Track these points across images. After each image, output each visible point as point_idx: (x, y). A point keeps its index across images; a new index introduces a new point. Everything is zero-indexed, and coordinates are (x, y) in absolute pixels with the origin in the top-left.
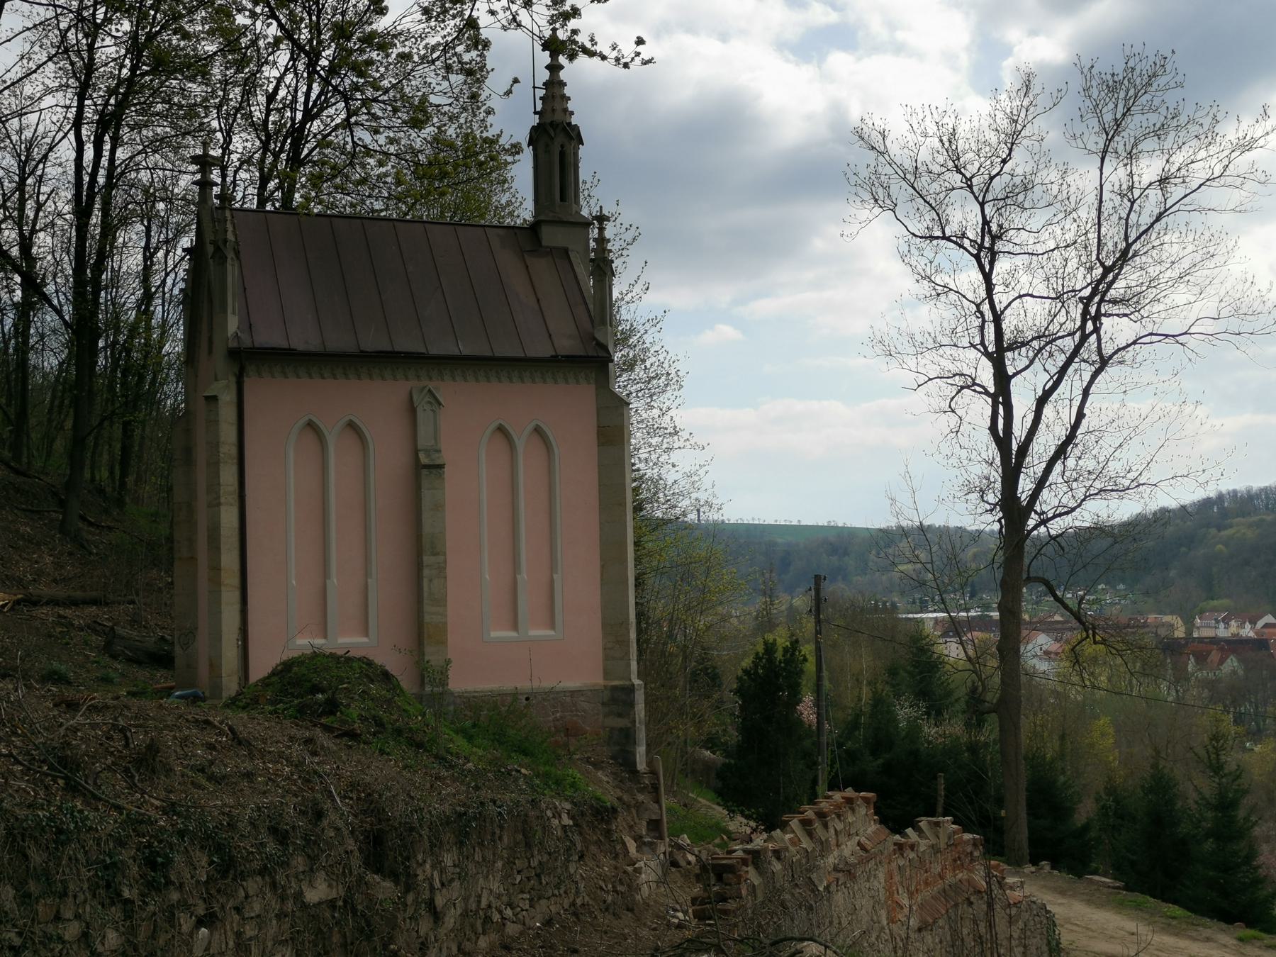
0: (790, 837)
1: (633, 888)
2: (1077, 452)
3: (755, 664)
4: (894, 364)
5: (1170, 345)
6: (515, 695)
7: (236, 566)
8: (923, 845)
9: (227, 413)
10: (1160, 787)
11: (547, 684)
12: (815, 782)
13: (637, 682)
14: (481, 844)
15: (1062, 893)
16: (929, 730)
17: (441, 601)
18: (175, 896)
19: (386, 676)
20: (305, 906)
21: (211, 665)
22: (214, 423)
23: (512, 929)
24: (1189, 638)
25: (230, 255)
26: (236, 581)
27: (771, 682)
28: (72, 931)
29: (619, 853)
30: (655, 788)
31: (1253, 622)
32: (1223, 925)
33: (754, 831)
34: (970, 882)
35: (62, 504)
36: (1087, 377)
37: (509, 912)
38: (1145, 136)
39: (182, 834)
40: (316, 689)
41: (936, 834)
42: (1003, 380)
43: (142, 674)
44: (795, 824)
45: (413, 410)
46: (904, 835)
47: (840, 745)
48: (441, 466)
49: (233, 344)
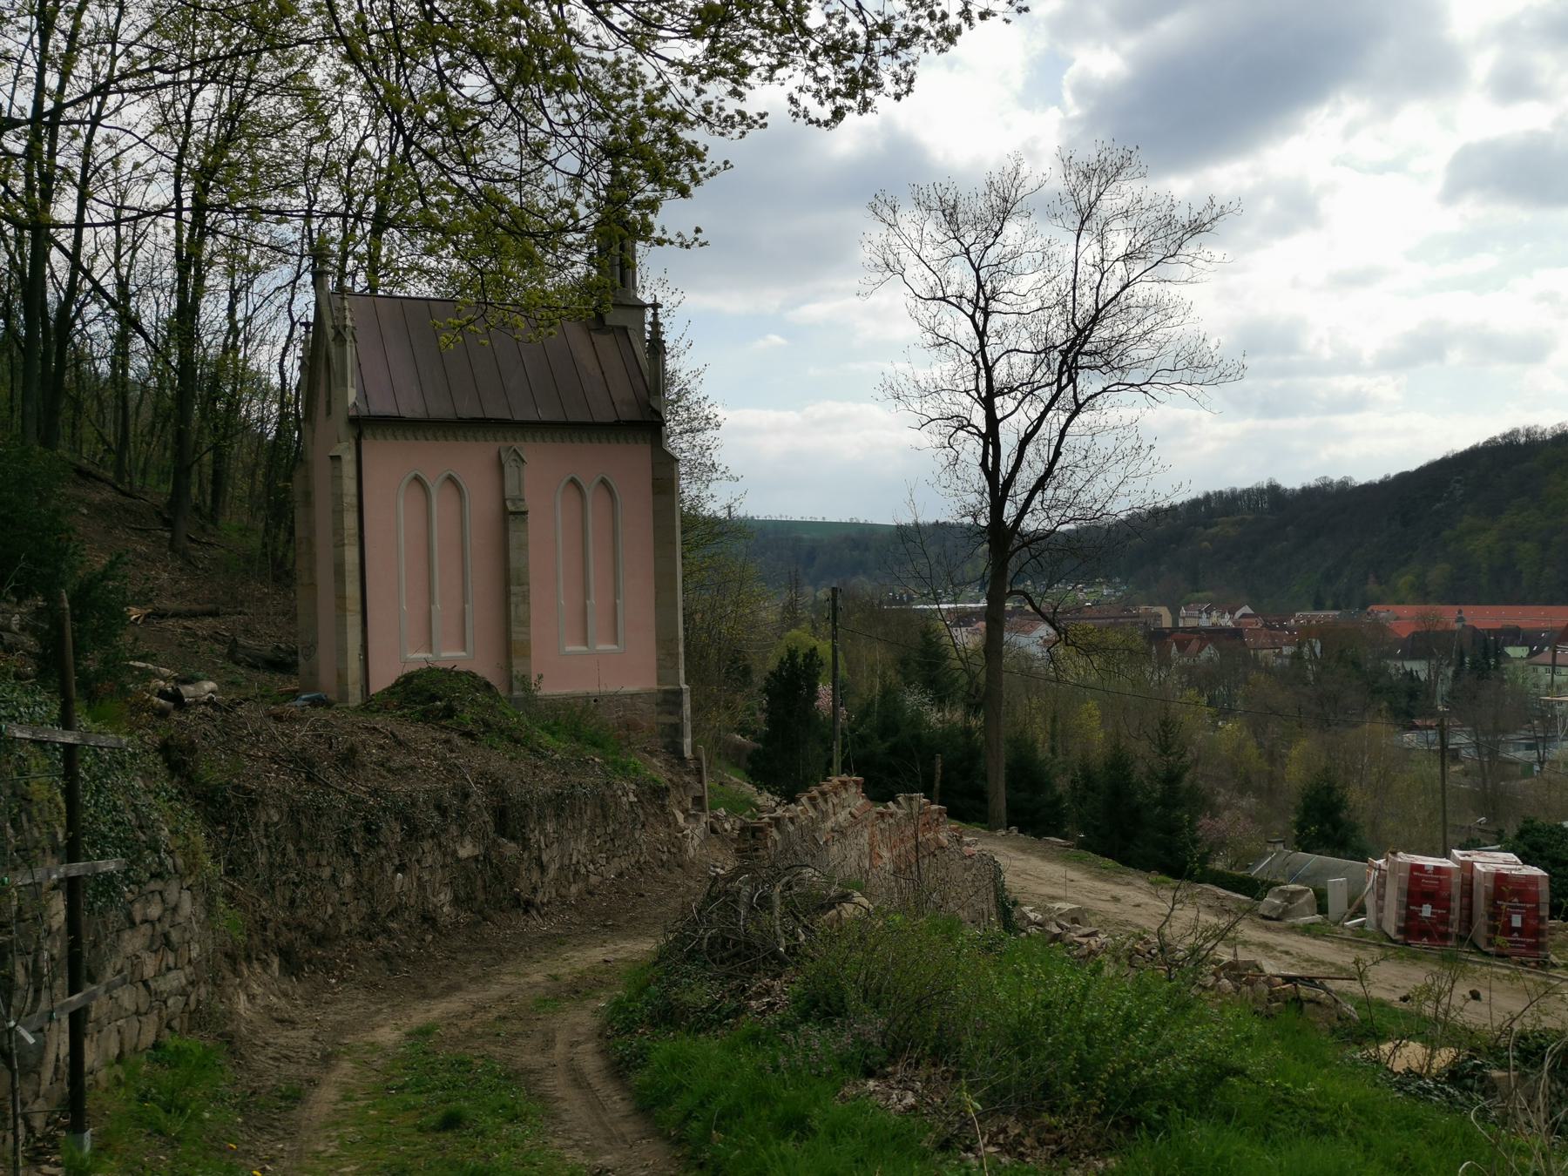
0: (802, 809)
1: (682, 850)
2: (1054, 483)
3: (780, 668)
4: (901, 406)
5: (1134, 395)
6: (587, 697)
7: (358, 595)
8: (901, 812)
9: (349, 469)
10: (1119, 763)
11: (612, 689)
12: (830, 763)
13: (684, 686)
14: (573, 817)
15: (1024, 851)
16: (934, 717)
17: (526, 623)
18: (383, 851)
19: (488, 686)
20: (458, 860)
21: (339, 676)
22: (337, 478)
23: (594, 879)
24: (1175, 629)
25: (349, 338)
26: (358, 607)
27: (793, 682)
28: (326, 873)
29: (670, 823)
30: (699, 772)
31: (1232, 613)
32: (1143, 873)
33: (778, 804)
34: (937, 840)
35: (169, 524)
36: (1063, 420)
37: (591, 867)
38: (1115, 216)
39: (385, 810)
40: (434, 698)
41: (911, 805)
42: (993, 422)
43: (264, 677)
44: (804, 800)
45: (501, 466)
46: (886, 807)
47: (853, 731)
48: (525, 513)
49: (353, 413)
